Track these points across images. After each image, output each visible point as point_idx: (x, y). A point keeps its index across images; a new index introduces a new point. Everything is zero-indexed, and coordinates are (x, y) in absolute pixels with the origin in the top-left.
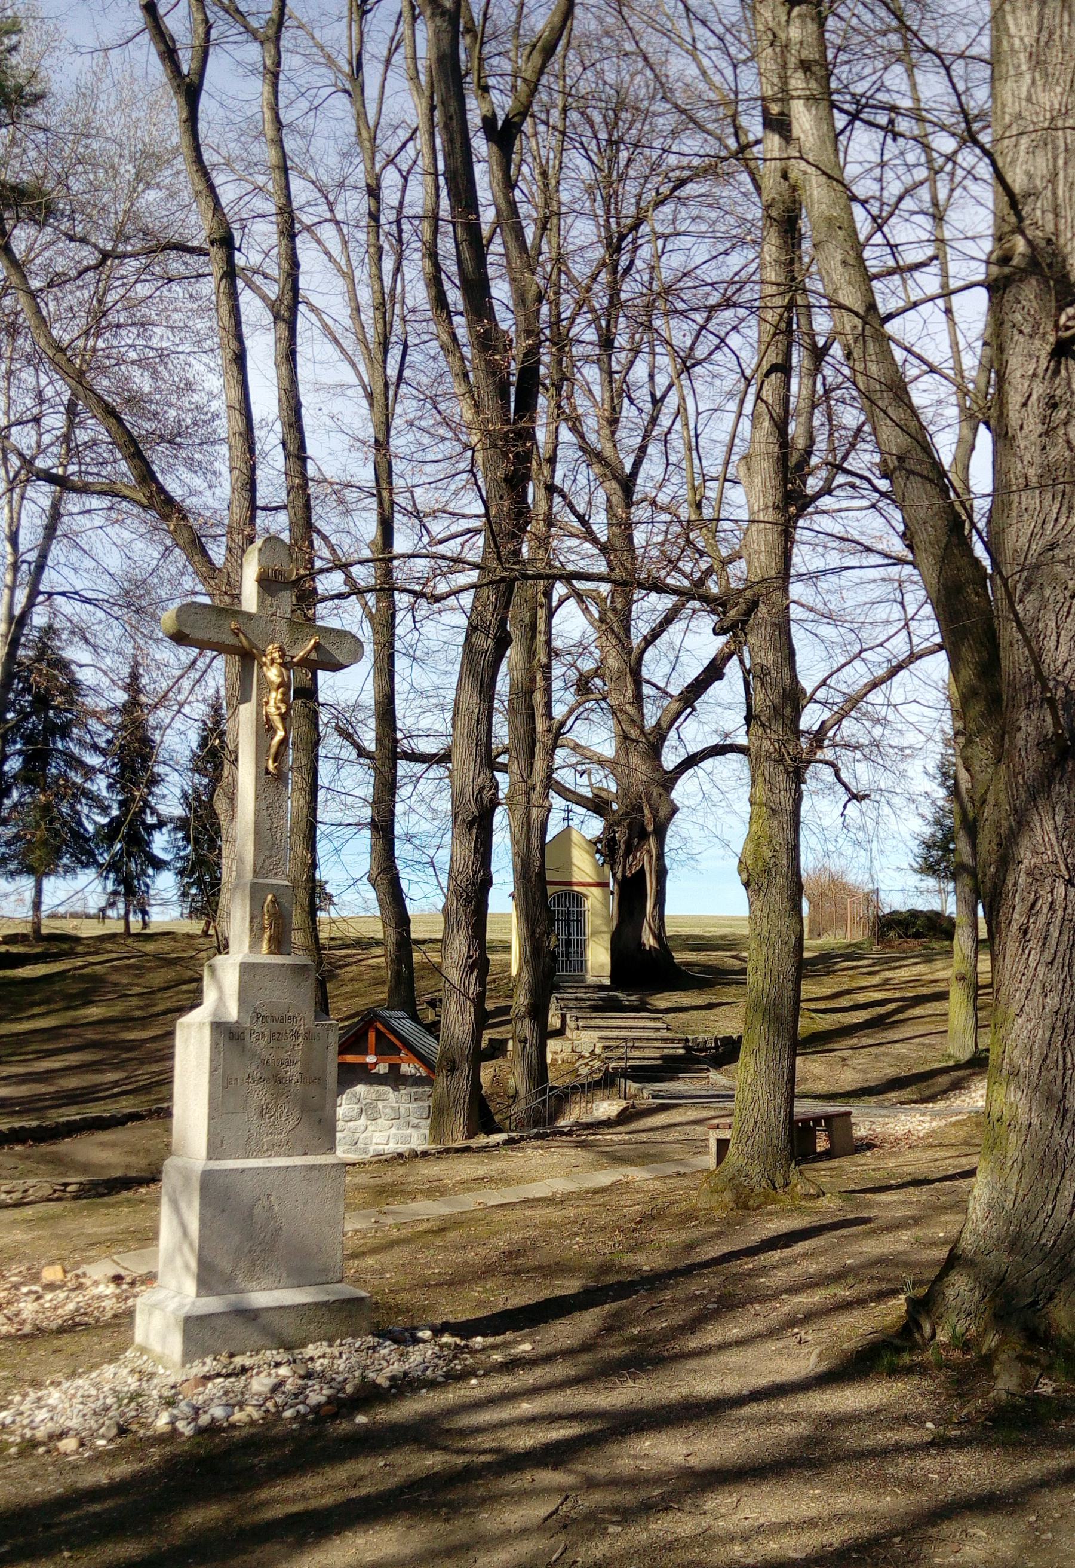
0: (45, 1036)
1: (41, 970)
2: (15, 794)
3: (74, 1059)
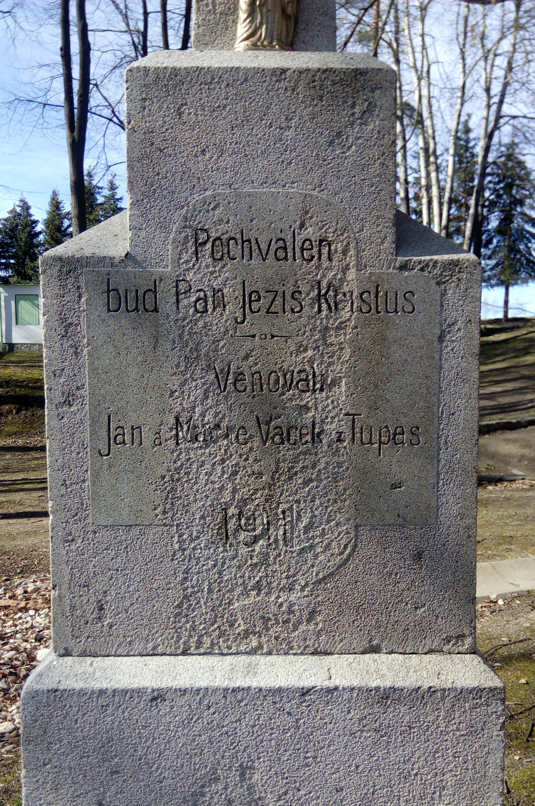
0: (498, 373)
1: (503, 336)
2: (495, 241)
3: (510, 386)
